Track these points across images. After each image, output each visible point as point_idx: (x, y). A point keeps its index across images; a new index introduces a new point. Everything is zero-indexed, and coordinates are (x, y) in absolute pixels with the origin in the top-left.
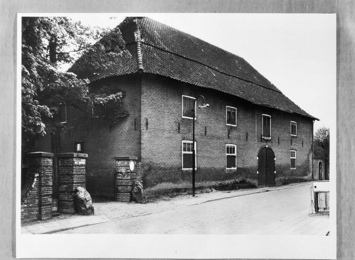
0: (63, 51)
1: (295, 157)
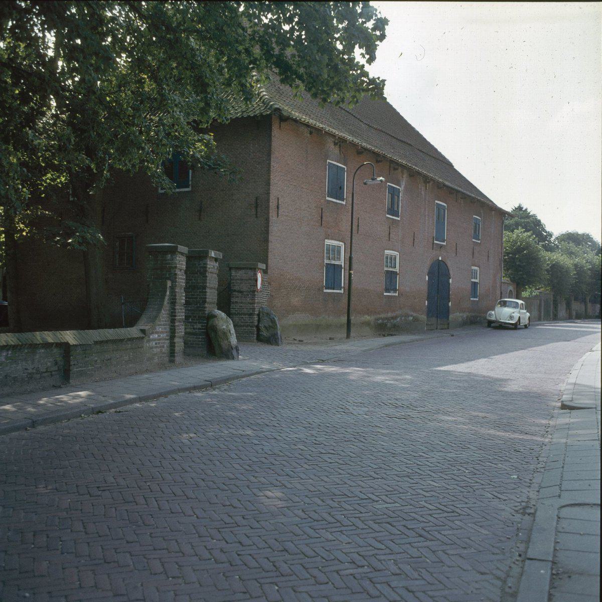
0: (160, 79)
1: (477, 279)
